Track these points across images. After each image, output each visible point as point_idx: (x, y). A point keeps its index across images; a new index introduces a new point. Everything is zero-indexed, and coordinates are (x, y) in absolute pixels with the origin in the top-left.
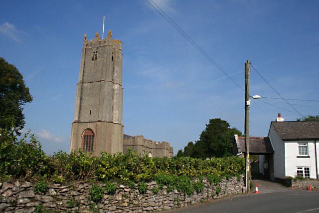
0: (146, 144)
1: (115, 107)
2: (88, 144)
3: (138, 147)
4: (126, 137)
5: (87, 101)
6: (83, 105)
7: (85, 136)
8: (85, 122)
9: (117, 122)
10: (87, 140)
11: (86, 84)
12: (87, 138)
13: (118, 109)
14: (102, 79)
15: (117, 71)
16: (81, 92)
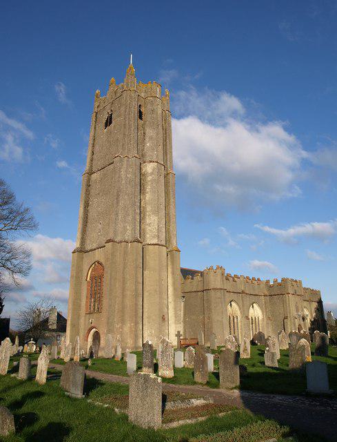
1: (149, 208)
3: (212, 293)
4: (186, 273)
5: (97, 205)
9: (155, 241)
13: (156, 212)
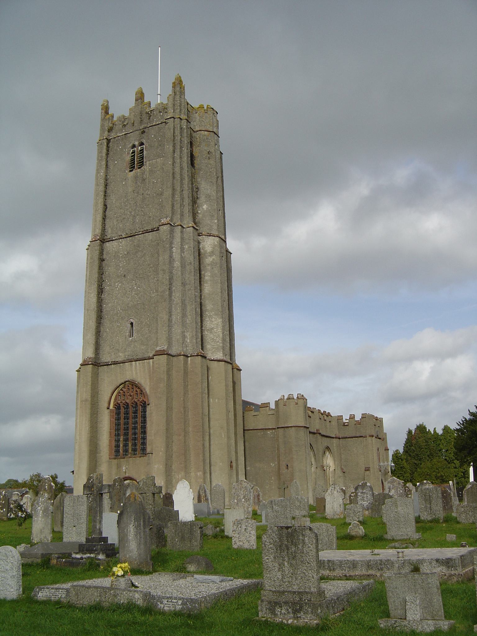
0: (316, 425)
2: (131, 432)
6: (106, 307)
7: (118, 407)
8: (115, 363)
10: (127, 418)
11: (115, 243)
12: (127, 413)
14: (164, 221)
15: (208, 197)
16: (101, 267)
